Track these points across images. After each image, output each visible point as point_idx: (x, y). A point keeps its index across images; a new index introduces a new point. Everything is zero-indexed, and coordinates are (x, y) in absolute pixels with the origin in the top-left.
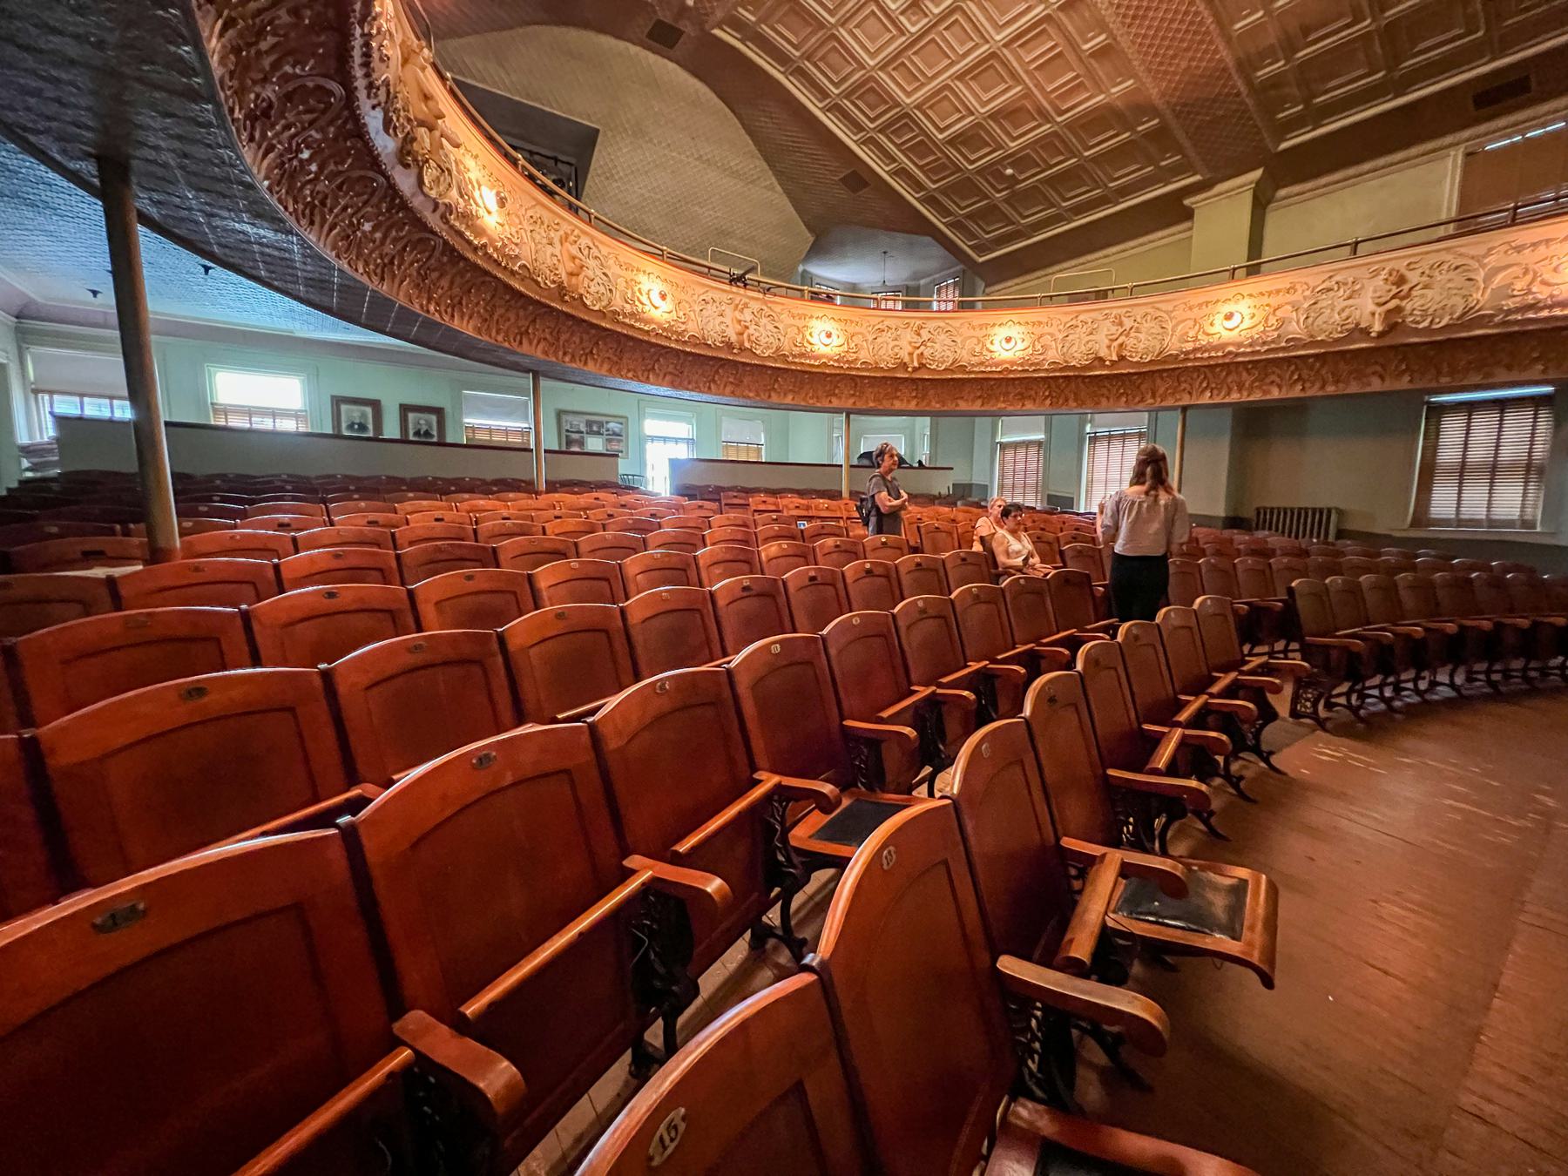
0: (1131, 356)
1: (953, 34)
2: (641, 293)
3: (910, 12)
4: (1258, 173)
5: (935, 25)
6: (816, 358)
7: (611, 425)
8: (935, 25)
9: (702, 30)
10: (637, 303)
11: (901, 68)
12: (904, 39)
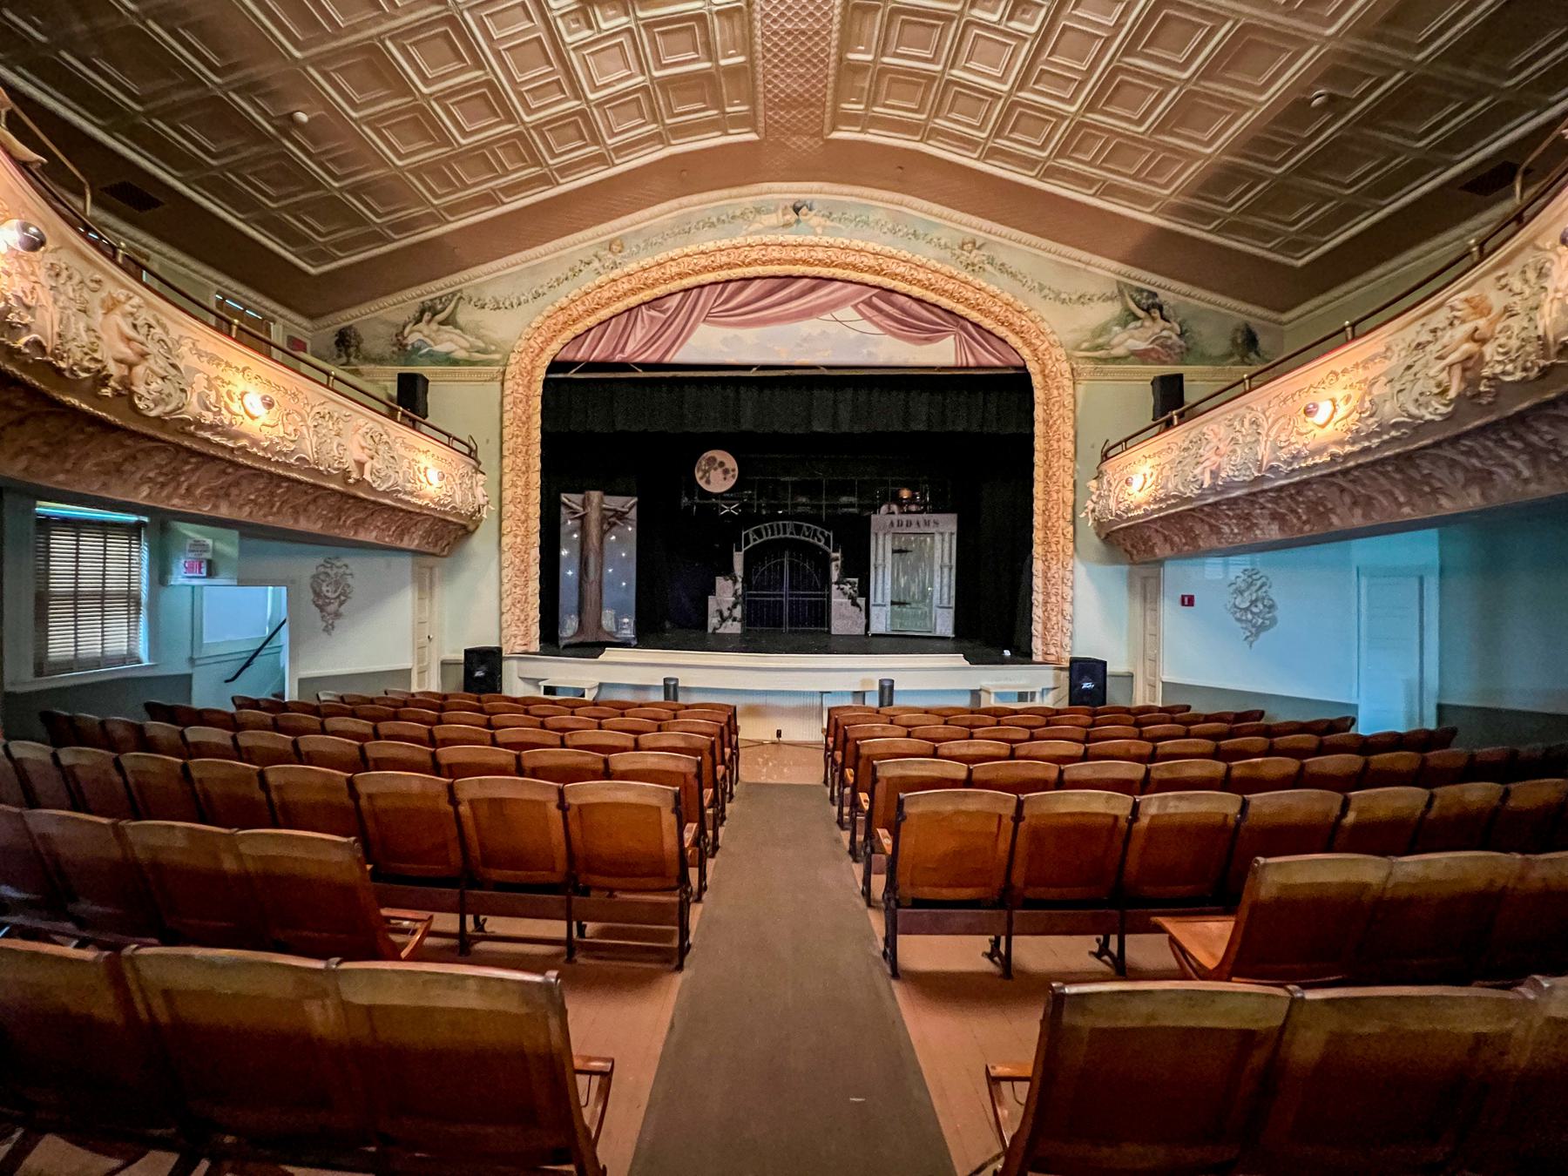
2: (232, 399)
3: (1018, 13)
10: (224, 411)
11: (1045, 77)
12: (1027, 45)
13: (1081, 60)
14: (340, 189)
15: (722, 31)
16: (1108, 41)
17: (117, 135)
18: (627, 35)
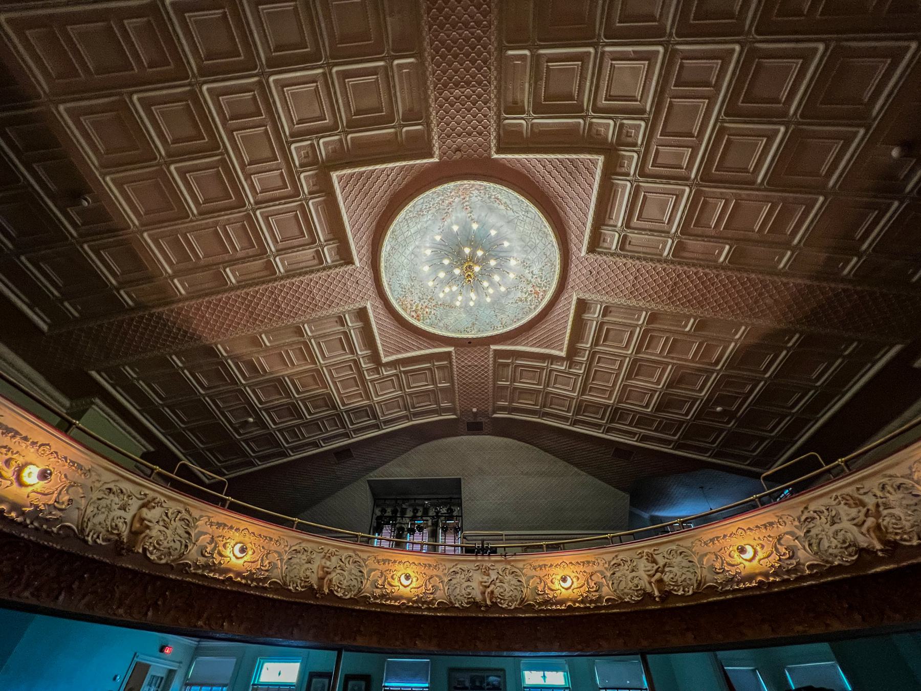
0: (501, 604)
1: (603, 363)
4: (152, 449)
5: (590, 364)
6: (561, 602)
7: (492, 679)
8: (590, 364)
9: (489, 418)
13: (608, 382)
14: (184, 429)
16: (617, 375)
17: (145, 414)
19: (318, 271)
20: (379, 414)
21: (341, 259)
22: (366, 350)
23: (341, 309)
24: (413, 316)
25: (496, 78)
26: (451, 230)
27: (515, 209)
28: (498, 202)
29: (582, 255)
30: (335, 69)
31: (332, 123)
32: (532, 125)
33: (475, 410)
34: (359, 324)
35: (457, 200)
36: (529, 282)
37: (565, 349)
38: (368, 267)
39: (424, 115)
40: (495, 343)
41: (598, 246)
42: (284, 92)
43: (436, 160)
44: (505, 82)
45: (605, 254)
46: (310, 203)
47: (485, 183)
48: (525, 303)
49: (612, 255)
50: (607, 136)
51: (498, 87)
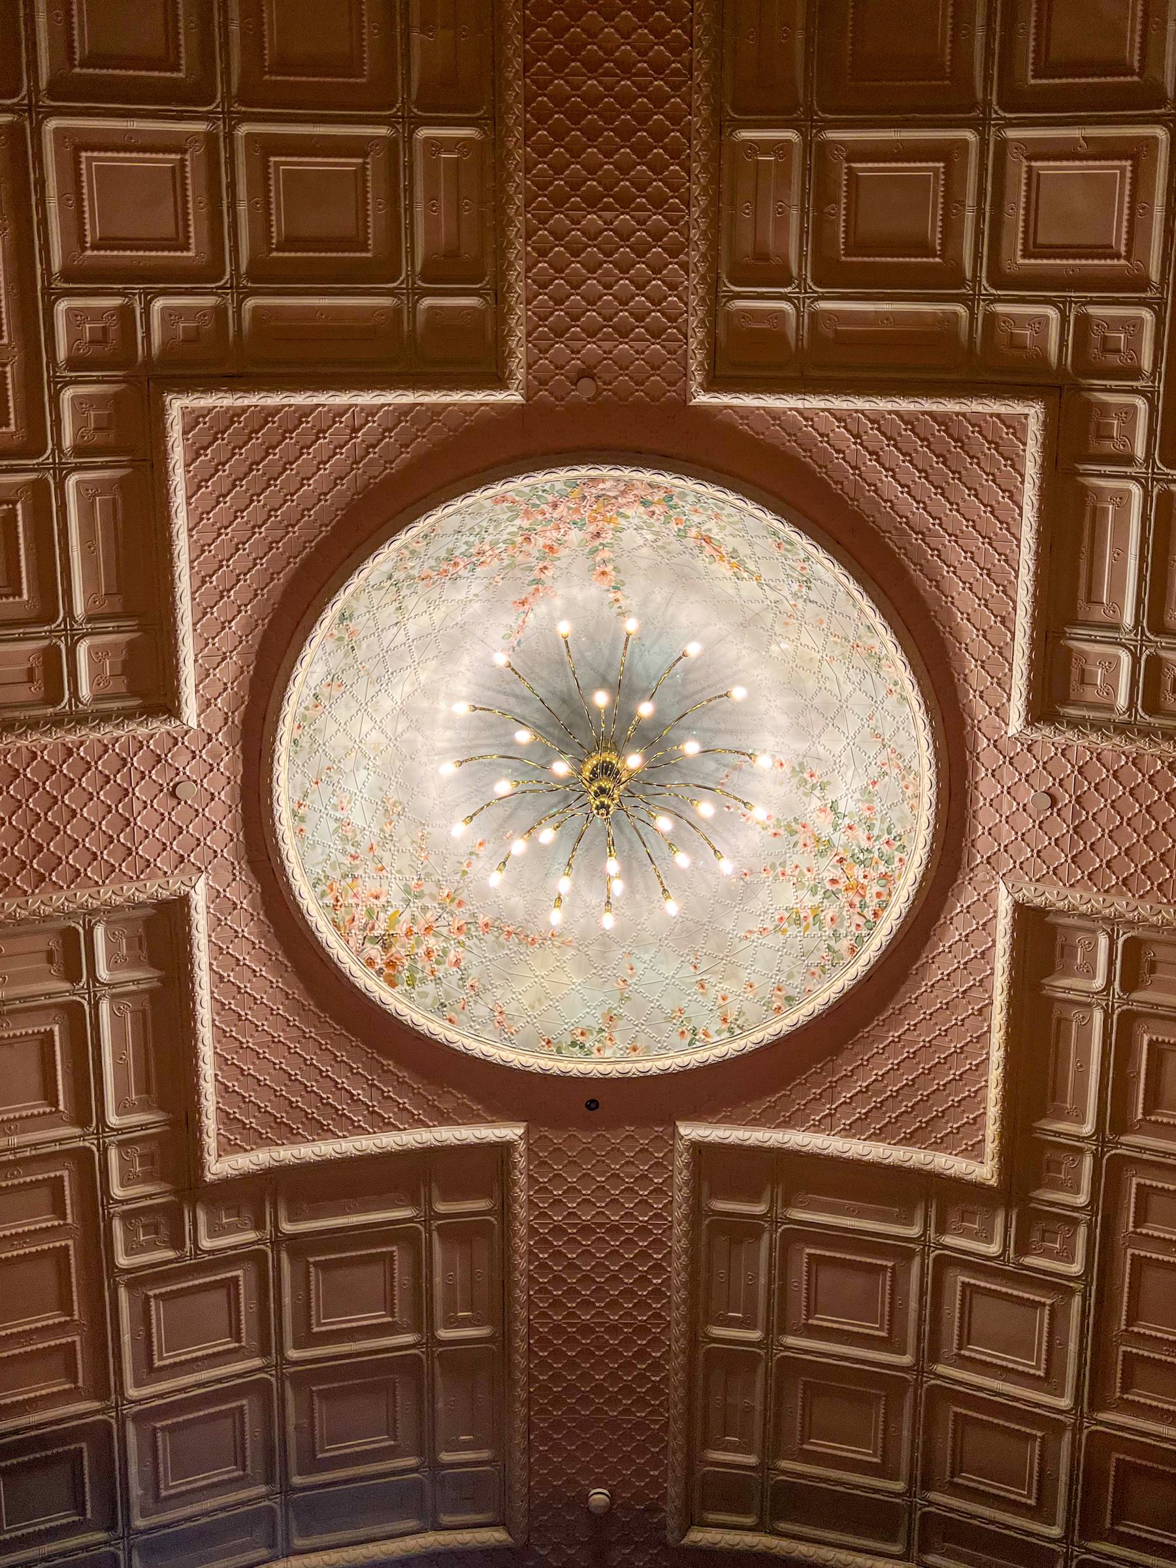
8: (1109, 1228)
15: (448, 1267)
18: (1007, 267)
19: (33, 725)
20: (136, 1491)
21: (132, 693)
22: (145, 1107)
23: (83, 896)
24: (370, 962)
25: (705, 191)
26: (552, 629)
27: (766, 576)
28: (707, 547)
29: (1012, 731)
30: (244, 129)
31: (204, 258)
32: (814, 315)
33: (599, 1497)
34: (141, 977)
35: (575, 536)
36: (824, 847)
37: (991, 1147)
38: (229, 734)
39: (490, 270)
40: (697, 1114)
41: (1066, 701)
42: (77, 162)
43: (514, 397)
44: (732, 204)
45: (1096, 726)
46: (71, 481)
47: (666, 480)
48: (814, 930)
49: (1121, 729)
50: (1045, 350)
51: (714, 214)
